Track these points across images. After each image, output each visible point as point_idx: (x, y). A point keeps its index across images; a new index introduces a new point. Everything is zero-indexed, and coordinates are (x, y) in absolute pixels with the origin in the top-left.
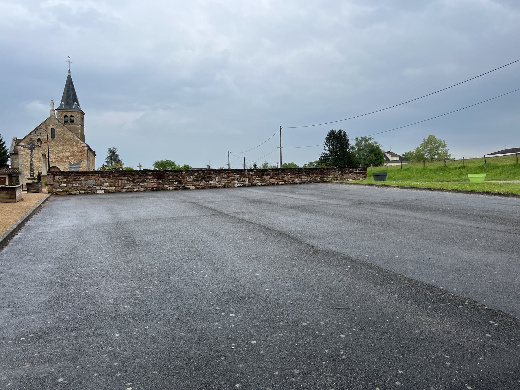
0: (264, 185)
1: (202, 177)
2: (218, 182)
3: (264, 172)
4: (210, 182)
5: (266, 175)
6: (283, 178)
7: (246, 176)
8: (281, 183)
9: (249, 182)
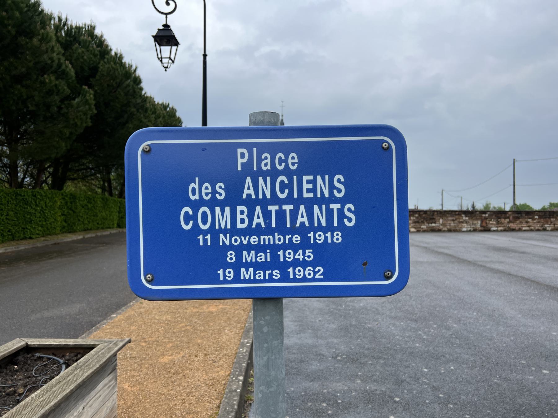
0: (501, 231)
1: (424, 218)
2: (442, 225)
3: (499, 214)
4: (433, 225)
5: (504, 218)
6: (527, 222)
7: (477, 219)
8: (524, 228)
9: (481, 226)
